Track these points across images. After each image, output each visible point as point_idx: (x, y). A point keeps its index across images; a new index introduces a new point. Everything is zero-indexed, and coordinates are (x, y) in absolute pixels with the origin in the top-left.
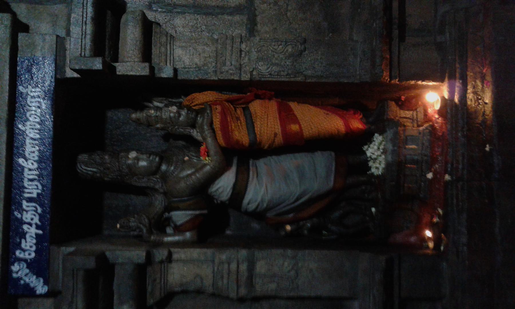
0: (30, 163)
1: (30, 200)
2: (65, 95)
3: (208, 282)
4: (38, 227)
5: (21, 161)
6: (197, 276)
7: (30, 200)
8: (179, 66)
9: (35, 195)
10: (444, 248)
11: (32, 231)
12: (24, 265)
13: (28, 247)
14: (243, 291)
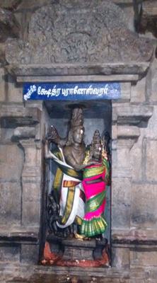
0: (76, 91)
1: (61, 91)
2: (107, 102)
3: (28, 164)
4: (50, 95)
5: (77, 87)
6: (30, 160)
7: (61, 91)
8: (118, 151)
9: (63, 93)
10: (91, 195)
11: (48, 93)
12: (35, 90)
13: (42, 92)
14: (24, 179)
